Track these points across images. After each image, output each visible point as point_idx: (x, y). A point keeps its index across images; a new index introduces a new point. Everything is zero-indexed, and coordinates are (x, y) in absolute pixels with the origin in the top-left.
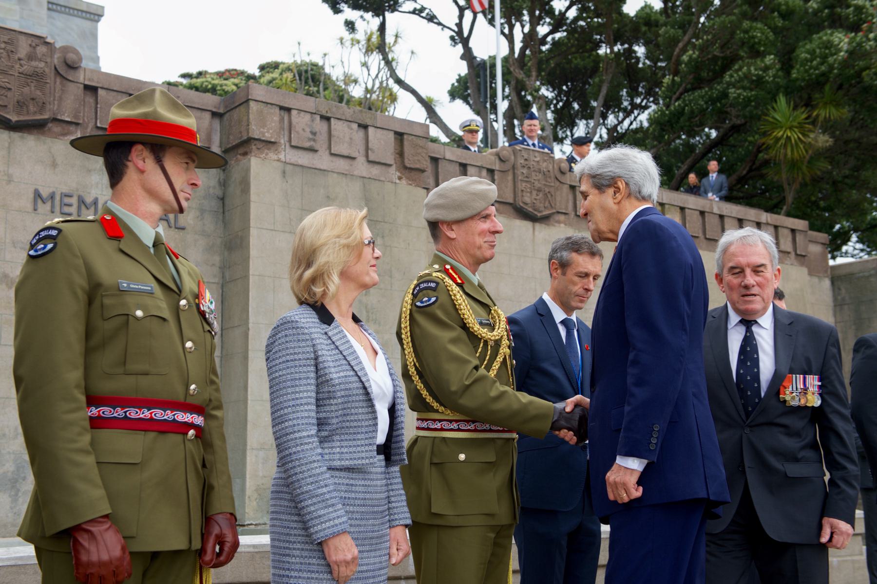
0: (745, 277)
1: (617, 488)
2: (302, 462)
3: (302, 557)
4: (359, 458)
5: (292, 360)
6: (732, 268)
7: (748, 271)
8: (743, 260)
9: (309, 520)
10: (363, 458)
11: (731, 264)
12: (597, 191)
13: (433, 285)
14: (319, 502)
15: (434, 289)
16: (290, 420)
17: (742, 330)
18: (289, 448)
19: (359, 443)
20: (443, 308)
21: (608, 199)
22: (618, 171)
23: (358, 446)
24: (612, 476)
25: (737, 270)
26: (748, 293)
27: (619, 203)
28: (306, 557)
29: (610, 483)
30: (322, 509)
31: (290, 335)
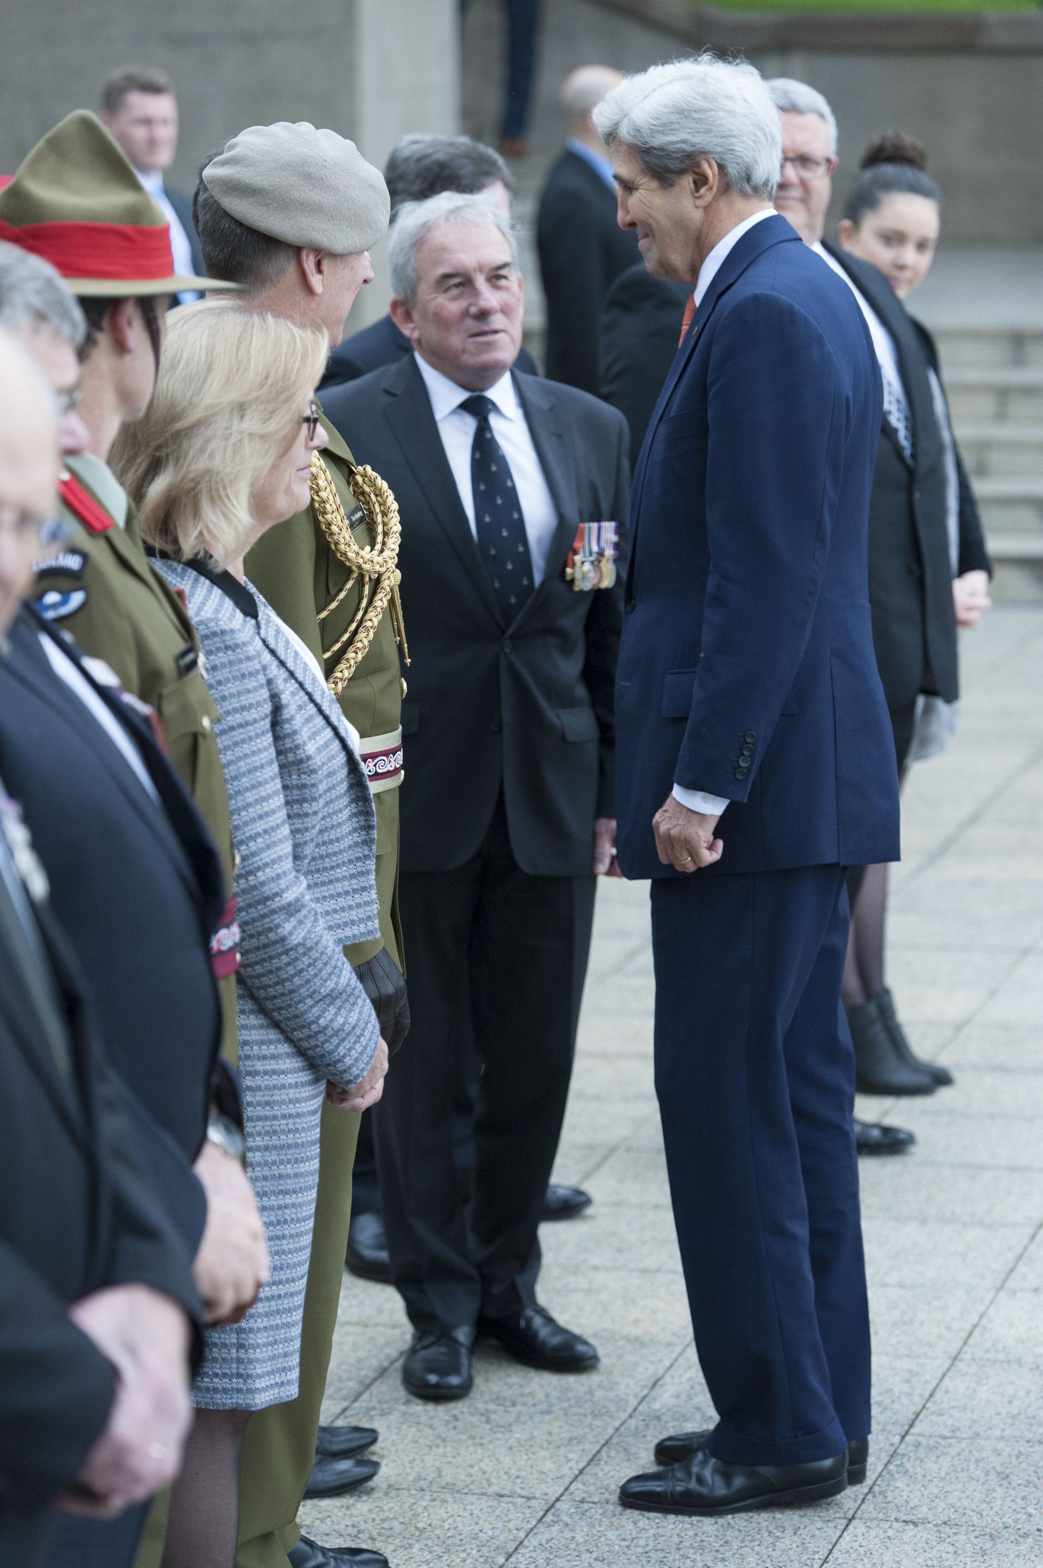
0: (475, 293)
1: (673, 847)
4: (346, 924)
5: (240, 726)
7: (481, 282)
10: (353, 922)
11: (441, 270)
12: (654, 184)
16: (267, 865)
17: (469, 424)
19: (339, 887)
21: (683, 203)
22: (699, 140)
23: (339, 895)
24: (664, 821)
25: (457, 280)
26: (485, 328)
27: (707, 208)
29: (659, 837)
31: (223, 665)
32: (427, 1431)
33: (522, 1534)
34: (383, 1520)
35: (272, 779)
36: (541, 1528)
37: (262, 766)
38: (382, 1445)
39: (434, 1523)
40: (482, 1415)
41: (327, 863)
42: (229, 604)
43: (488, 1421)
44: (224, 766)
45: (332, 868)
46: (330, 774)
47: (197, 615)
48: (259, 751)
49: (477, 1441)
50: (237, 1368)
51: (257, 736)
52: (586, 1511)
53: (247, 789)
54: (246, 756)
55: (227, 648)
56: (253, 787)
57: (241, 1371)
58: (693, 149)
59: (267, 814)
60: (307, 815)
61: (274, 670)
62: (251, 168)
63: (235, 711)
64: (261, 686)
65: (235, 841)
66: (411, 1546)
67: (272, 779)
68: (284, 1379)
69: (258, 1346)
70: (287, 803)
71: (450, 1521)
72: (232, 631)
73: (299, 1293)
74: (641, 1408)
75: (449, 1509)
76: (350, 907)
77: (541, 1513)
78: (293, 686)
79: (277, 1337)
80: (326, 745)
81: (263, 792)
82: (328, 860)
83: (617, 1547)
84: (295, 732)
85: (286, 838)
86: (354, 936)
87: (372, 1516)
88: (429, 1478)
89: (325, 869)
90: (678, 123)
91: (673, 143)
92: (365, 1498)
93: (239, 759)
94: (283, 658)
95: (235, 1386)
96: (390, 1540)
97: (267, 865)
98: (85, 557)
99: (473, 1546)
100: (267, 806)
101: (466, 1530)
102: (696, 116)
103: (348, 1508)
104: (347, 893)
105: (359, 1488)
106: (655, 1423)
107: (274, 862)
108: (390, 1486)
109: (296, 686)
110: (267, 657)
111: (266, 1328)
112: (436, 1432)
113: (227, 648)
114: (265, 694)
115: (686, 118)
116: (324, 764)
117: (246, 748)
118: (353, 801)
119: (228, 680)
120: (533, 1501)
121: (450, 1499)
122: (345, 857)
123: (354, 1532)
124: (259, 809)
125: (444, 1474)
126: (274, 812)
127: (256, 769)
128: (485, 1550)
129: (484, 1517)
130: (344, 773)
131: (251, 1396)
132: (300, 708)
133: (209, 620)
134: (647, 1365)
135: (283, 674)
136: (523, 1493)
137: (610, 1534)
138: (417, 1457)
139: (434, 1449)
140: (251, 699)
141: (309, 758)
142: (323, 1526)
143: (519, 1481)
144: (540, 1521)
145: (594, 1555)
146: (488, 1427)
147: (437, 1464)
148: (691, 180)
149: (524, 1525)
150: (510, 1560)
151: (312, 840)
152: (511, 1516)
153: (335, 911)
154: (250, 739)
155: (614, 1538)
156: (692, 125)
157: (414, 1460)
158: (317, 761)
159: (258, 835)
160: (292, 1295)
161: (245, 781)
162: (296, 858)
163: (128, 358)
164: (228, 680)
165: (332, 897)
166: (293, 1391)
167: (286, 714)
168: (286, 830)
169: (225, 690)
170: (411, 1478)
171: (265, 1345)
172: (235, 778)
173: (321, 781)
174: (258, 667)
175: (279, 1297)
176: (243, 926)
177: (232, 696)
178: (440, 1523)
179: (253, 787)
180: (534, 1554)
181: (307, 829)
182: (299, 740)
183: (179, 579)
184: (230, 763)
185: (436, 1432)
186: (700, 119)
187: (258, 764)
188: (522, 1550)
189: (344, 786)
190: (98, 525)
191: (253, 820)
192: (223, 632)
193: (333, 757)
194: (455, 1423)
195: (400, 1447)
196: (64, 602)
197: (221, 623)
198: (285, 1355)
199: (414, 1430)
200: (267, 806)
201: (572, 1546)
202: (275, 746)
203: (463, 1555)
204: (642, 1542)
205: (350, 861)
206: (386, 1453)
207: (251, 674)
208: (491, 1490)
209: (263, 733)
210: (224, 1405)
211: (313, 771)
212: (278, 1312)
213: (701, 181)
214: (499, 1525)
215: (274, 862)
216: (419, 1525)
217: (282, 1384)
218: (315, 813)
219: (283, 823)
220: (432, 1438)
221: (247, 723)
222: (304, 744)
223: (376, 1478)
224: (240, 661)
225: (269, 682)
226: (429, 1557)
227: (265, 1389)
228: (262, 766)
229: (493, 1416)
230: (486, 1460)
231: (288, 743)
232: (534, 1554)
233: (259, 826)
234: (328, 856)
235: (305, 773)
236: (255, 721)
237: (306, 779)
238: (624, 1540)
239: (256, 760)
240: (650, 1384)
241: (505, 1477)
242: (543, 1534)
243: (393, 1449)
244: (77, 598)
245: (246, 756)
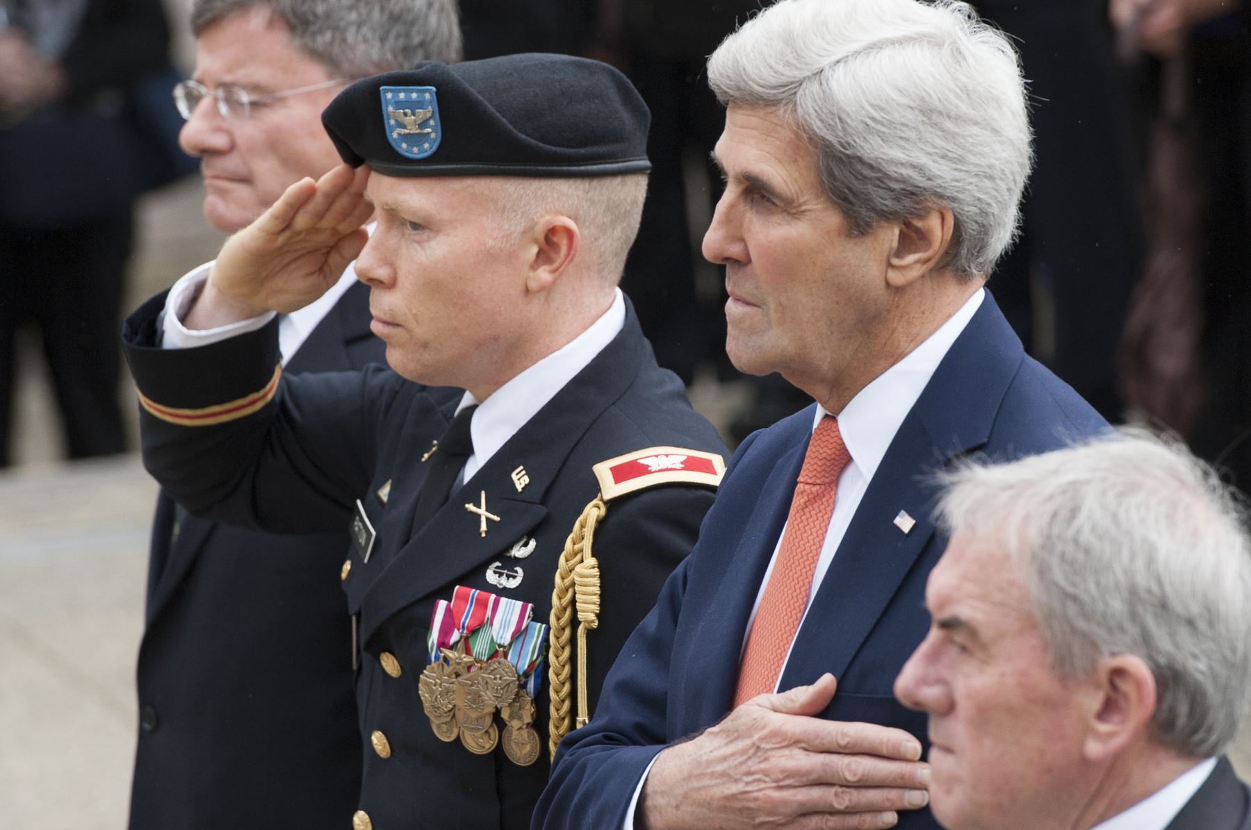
58: (928, 184)
62: (505, 715)
90: (916, 129)
91: (892, 162)
102: (948, 125)
115: (935, 125)
148: (897, 231)
156: (939, 142)
186: (954, 135)
213: (912, 238)
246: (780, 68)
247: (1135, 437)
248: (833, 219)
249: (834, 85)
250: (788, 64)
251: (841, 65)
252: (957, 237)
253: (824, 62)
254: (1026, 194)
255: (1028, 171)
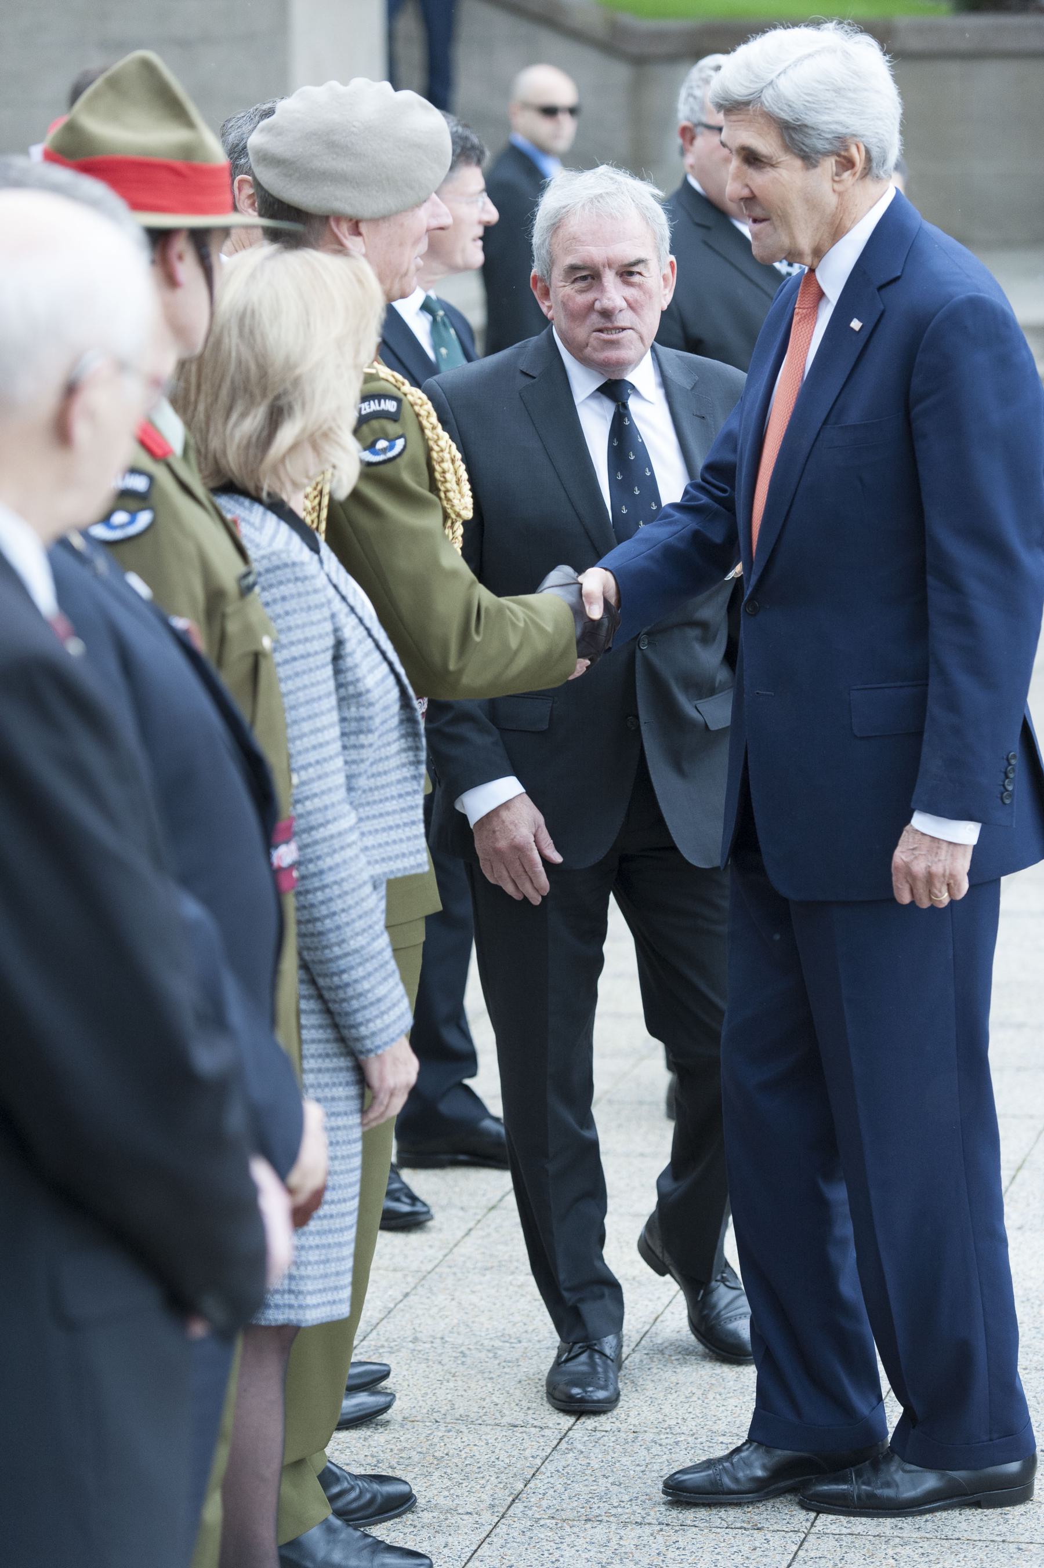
0: (602, 289)
2: (346, 886)
3: (319, 1085)
5: (303, 657)
6: (573, 268)
7: (610, 279)
8: (595, 252)
9: (356, 1011)
11: (570, 260)
13: (390, 406)
14: (376, 970)
15: (394, 417)
16: (315, 795)
17: (608, 409)
18: (319, 858)
19: (390, 821)
20: (413, 466)
23: (391, 828)
26: (609, 325)
28: (327, 1085)
30: (380, 983)
32: (437, 1367)
33: (539, 1462)
34: (401, 1450)
35: (329, 711)
36: (556, 1455)
37: (320, 698)
38: (395, 1380)
39: (451, 1452)
40: (489, 1351)
41: (376, 795)
42: (296, 539)
43: (495, 1357)
44: (284, 695)
45: (381, 801)
46: (385, 708)
47: (270, 545)
48: (318, 683)
49: (486, 1375)
50: (289, 1284)
51: (318, 668)
52: (599, 1439)
53: (304, 720)
54: (305, 687)
55: (297, 579)
56: (310, 717)
57: (293, 1287)
58: (848, 131)
59: (321, 745)
60: (362, 746)
61: (338, 605)
63: (299, 642)
64: (325, 619)
65: (294, 766)
66: (430, 1474)
67: (329, 711)
68: (337, 1298)
69: (309, 1263)
70: (343, 734)
71: (467, 1450)
72: (302, 564)
73: (350, 1213)
74: (643, 1342)
75: (464, 1439)
76: (401, 840)
77: (555, 1442)
78: (353, 620)
79: (329, 1256)
80: (383, 680)
81: (318, 723)
82: (376, 793)
83: (632, 1472)
84: (356, 666)
85: (339, 770)
86: (405, 869)
87: (389, 1446)
88: (443, 1412)
89: (375, 802)
92: (381, 1430)
93: (299, 689)
94: (344, 592)
95: (287, 1302)
96: (409, 1468)
97: (315, 795)
98: (151, 478)
99: (492, 1473)
100: (321, 738)
101: (483, 1459)
103: (365, 1439)
104: (398, 826)
105: (375, 1420)
106: (659, 1356)
107: (323, 793)
108: (404, 1418)
109: (356, 621)
110: (331, 591)
111: (317, 1247)
112: (445, 1368)
113: (297, 579)
114: (328, 627)
116: (381, 698)
117: (306, 679)
118: (403, 736)
119: (295, 611)
120: (546, 1430)
121: (464, 1429)
122: (394, 791)
123: (374, 1461)
124: (312, 740)
125: (456, 1406)
126: (328, 743)
127: (313, 700)
128: (503, 1476)
129: (499, 1446)
130: (396, 708)
131: (301, 1312)
132: (360, 642)
133: (281, 552)
134: (646, 1302)
135: (345, 609)
136: (536, 1423)
137: (624, 1460)
138: (429, 1391)
139: (445, 1383)
140: (313, 631)
141: (368, 691)
142: (343, 1456)
143: (530, 1412)
144: (554, 1449)
145: (611, 1480)
146: (497, 1362)
147: (449, 1397)
149: (539, 1453)
150: (529, 1486)
151: (366, 772)
152: (526, 1445)
153: (387, 843)
154: (311, 670)
155: (628, 1463)
157: (426, 1394)
158: (374, 696)
159: (310, 765)
160: (343, 1215)
161: (303, 712)
162: (350, 789)
163: (180, 293)
164: (295, 611)
165: (384, 830)
166: (343, 1310)
167: (349, 647)
168: (339, 762)
169: (291, 621)
170: (425, 1411)
171: (317, 1263)
172: (293, 708)
173: (377, 714)
174: (324, 600)
175: (332, 1216)
176: (301, 848)
177: (298, 627)
178: (457, 1452)
179: (310, 717)
180: (552, 1480)
181: (362, 761)
182: (360, 672)
183: (247, 512)
184: (290, 692)
185: (445, 1368)
187: (316, 696)
188: (539, 1476)
189: (395, 721)
190: (159, 451)
191: (307, 750)
192: (294, 564)
193: (388, 692)
194: (464, 1359)
195: (411, 1382)
196: (132, 521)
197: (293, 555)
198: (338, 1274)
199: (424, 1365)
200: (321, 738)
201: (588, 1472)
202: (336, 680)
203: (482, 1482)
204: (656, 1467)
205: (400, 796)
206: (398, 1387)
207: (317, 607)
208: (504, 1421)
209: (324, 666)
210: (276, 1320)
211: (371, 704)
212: (330, 1231)
214: (515, 1453)
215: (323, 793)
216: (436, 1454)
217: (334, 1302)
218: (371, 745)
219: (337, 755)
220: (442, 1373)
221: (309, 655)
222: (364, 677)
223: (390, 1411)
224: (308, 593)
225: (333, 616)
226: (449, 1483)
227: (317, 1306)
228: (320, 698)
229: (500, 1352)
230: (497, 1393)
231: (350, 677)
232: (552, 1480)
233: (312, 757)
234: (377, 788)
235: (363, 706)
236: (316, 653)
237: (365, 712)
238: (638, 1465)
239: (314, 692)
240: (651, 1321)
241: (517, 1408)
242: (559, 1461)
243: (405, 1384)
244: (144, 518)
245: (305, 687)
246: (748, 84)
247: (93, 203)
248: (798, 163)
249: (781, 88)
250: (752, 81)
251: (782, 76)
252: (869, 159)
253: (773, 76)
254: (902, 124)
255: (900, 111)
